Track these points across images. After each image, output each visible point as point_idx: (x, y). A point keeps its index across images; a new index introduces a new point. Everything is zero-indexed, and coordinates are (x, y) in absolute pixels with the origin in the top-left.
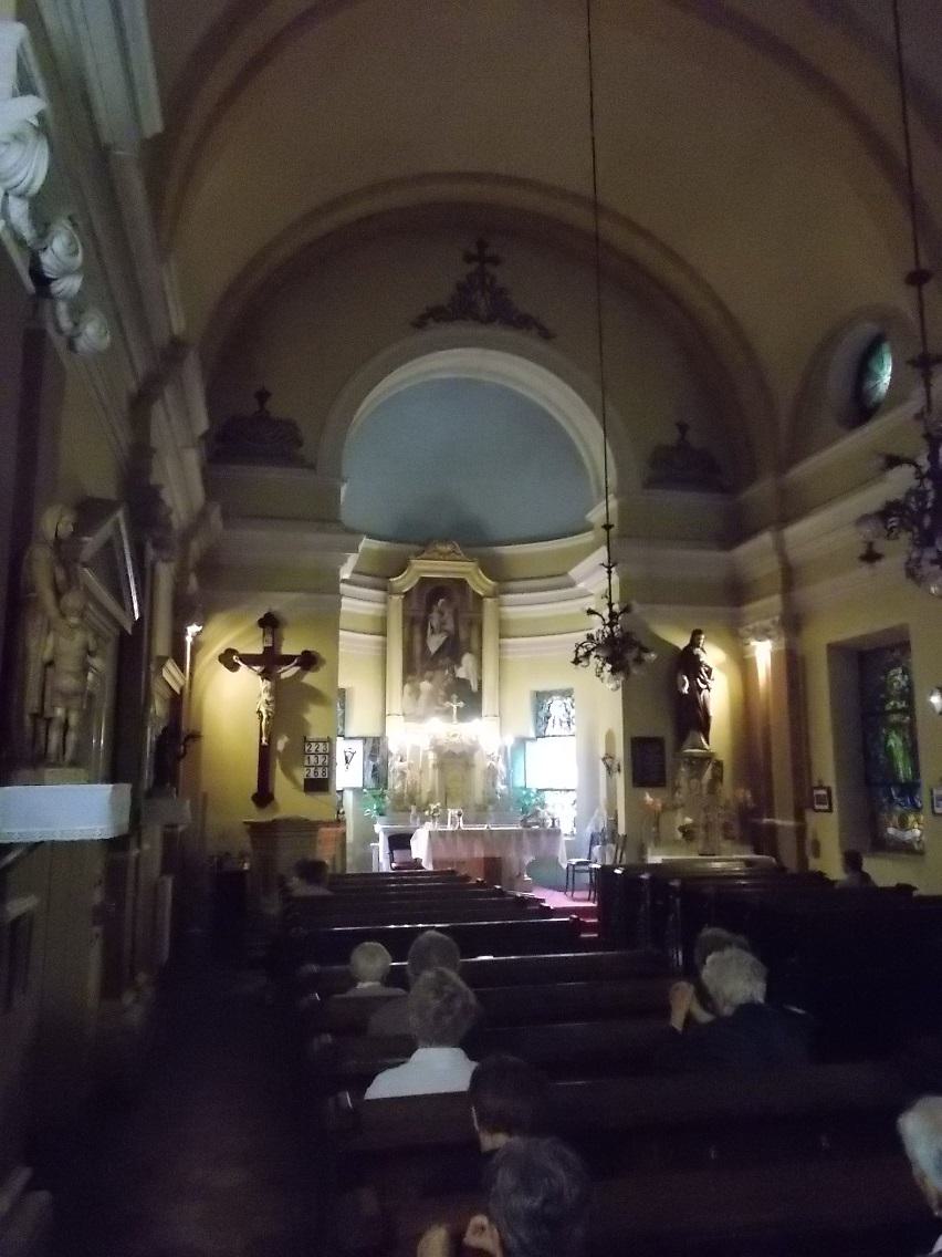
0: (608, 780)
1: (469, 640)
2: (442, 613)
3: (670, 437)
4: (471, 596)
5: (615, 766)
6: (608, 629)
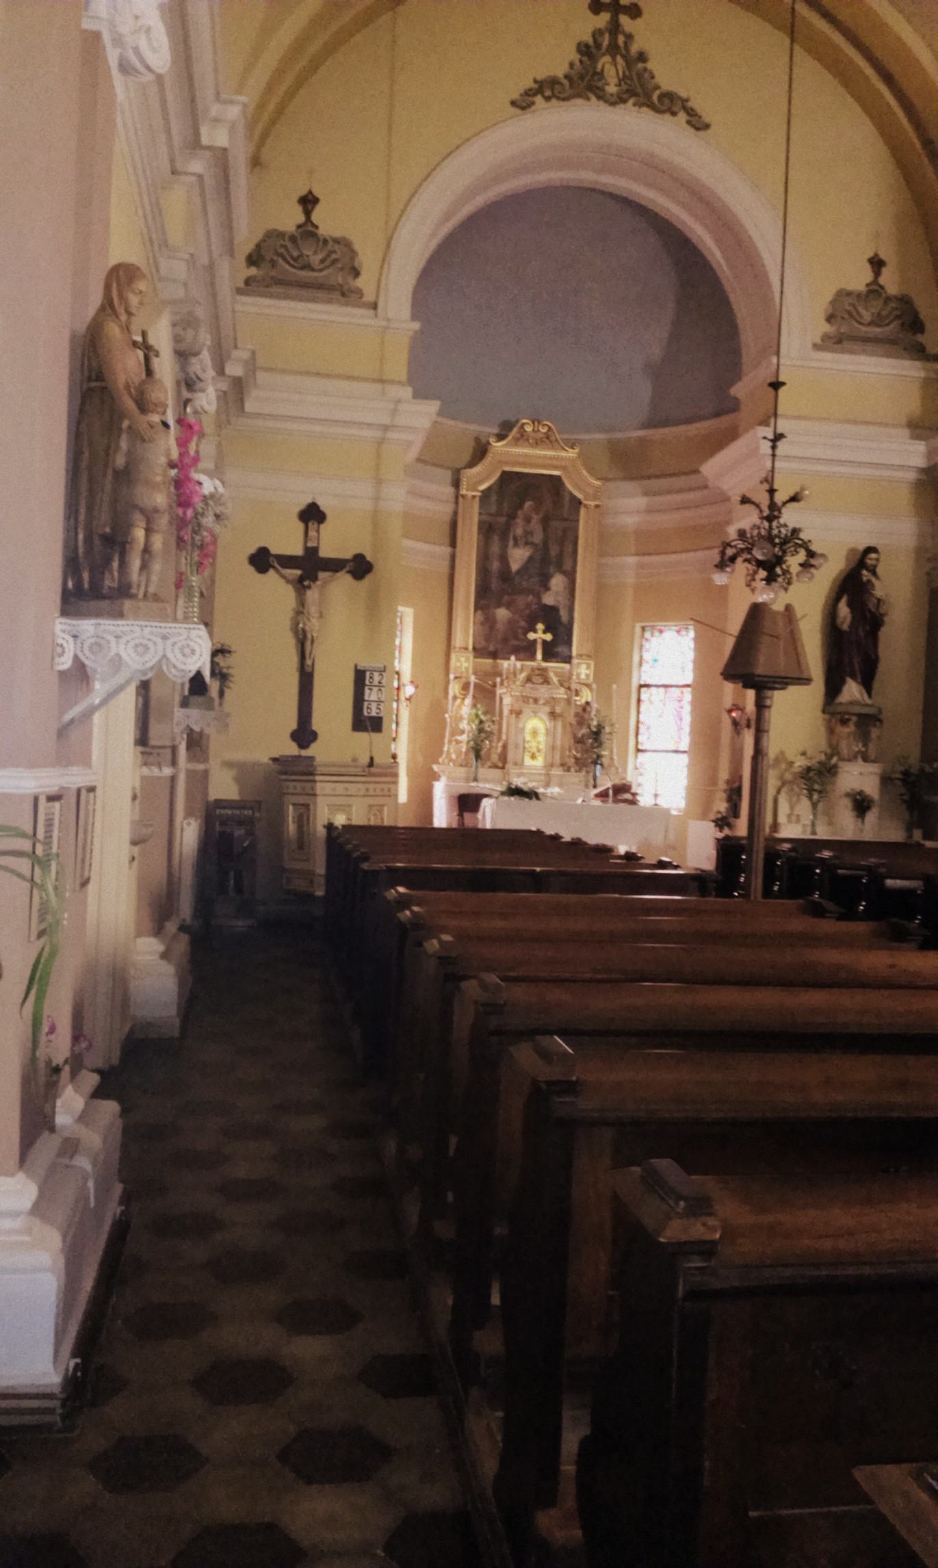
0: (733, 738)
1: (560, 555)
2: (528, 520)
3: (860, 279)
4: (567, 499)
5: (744, 722)
6: (766, 524)
